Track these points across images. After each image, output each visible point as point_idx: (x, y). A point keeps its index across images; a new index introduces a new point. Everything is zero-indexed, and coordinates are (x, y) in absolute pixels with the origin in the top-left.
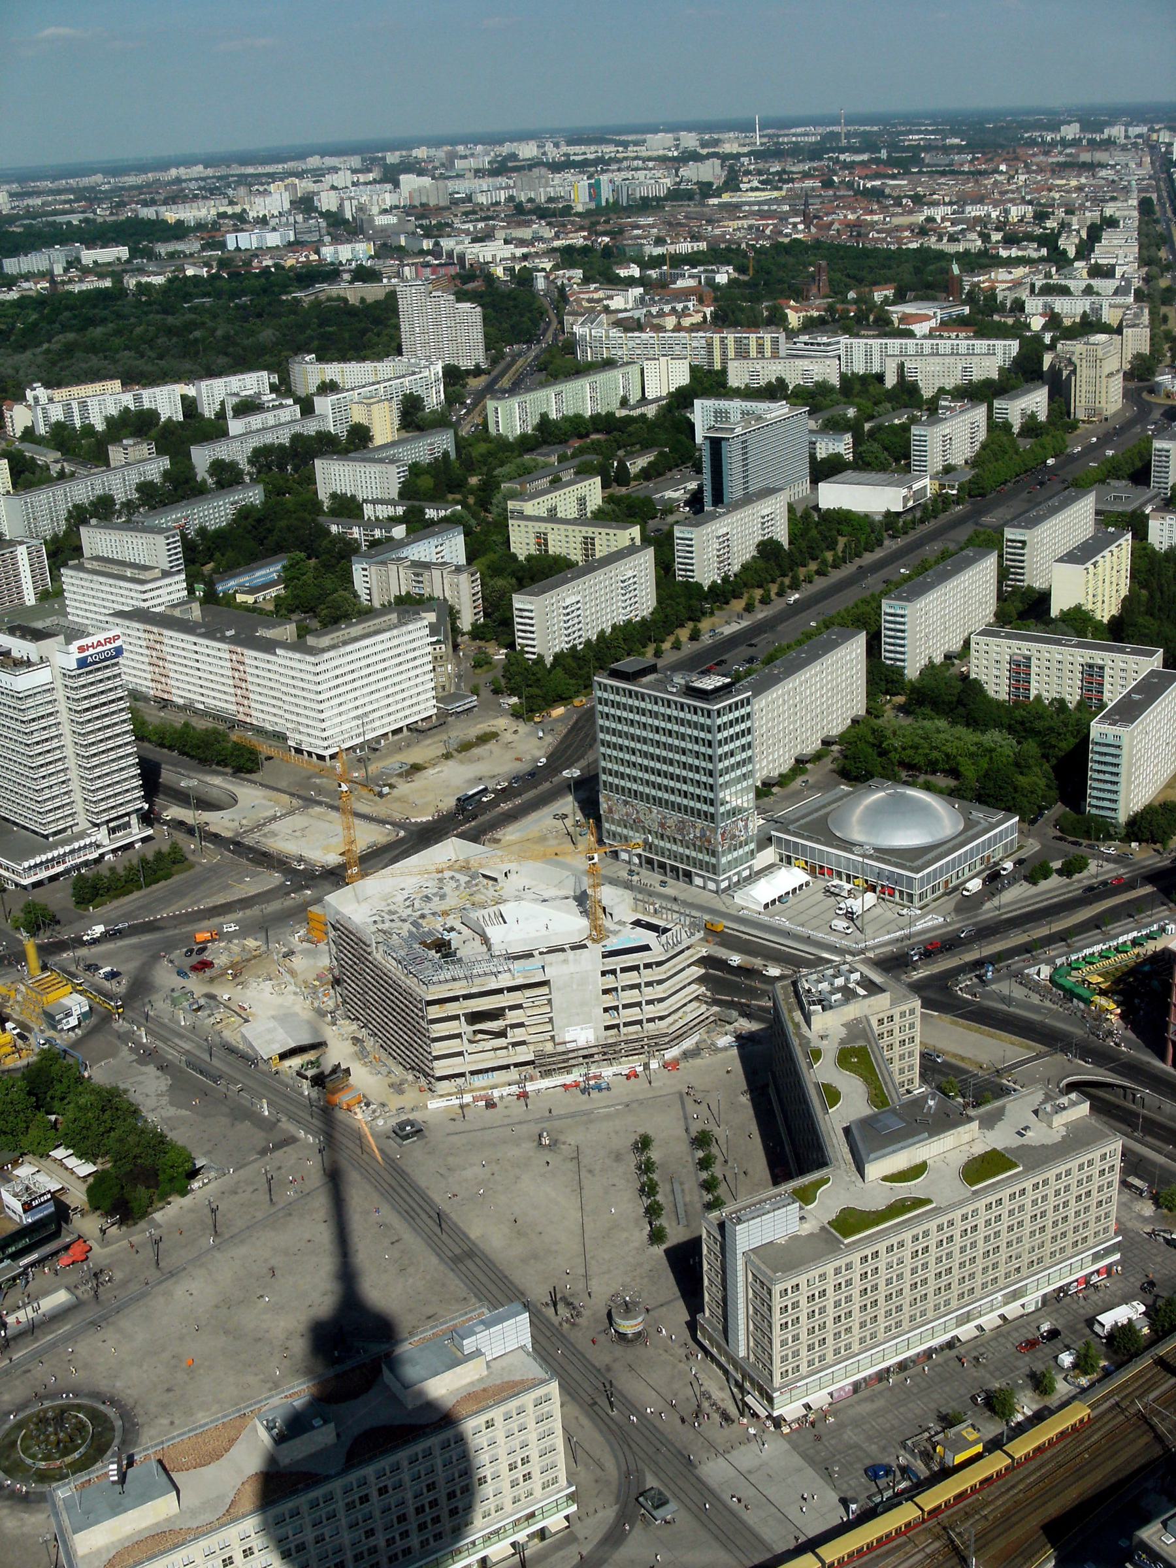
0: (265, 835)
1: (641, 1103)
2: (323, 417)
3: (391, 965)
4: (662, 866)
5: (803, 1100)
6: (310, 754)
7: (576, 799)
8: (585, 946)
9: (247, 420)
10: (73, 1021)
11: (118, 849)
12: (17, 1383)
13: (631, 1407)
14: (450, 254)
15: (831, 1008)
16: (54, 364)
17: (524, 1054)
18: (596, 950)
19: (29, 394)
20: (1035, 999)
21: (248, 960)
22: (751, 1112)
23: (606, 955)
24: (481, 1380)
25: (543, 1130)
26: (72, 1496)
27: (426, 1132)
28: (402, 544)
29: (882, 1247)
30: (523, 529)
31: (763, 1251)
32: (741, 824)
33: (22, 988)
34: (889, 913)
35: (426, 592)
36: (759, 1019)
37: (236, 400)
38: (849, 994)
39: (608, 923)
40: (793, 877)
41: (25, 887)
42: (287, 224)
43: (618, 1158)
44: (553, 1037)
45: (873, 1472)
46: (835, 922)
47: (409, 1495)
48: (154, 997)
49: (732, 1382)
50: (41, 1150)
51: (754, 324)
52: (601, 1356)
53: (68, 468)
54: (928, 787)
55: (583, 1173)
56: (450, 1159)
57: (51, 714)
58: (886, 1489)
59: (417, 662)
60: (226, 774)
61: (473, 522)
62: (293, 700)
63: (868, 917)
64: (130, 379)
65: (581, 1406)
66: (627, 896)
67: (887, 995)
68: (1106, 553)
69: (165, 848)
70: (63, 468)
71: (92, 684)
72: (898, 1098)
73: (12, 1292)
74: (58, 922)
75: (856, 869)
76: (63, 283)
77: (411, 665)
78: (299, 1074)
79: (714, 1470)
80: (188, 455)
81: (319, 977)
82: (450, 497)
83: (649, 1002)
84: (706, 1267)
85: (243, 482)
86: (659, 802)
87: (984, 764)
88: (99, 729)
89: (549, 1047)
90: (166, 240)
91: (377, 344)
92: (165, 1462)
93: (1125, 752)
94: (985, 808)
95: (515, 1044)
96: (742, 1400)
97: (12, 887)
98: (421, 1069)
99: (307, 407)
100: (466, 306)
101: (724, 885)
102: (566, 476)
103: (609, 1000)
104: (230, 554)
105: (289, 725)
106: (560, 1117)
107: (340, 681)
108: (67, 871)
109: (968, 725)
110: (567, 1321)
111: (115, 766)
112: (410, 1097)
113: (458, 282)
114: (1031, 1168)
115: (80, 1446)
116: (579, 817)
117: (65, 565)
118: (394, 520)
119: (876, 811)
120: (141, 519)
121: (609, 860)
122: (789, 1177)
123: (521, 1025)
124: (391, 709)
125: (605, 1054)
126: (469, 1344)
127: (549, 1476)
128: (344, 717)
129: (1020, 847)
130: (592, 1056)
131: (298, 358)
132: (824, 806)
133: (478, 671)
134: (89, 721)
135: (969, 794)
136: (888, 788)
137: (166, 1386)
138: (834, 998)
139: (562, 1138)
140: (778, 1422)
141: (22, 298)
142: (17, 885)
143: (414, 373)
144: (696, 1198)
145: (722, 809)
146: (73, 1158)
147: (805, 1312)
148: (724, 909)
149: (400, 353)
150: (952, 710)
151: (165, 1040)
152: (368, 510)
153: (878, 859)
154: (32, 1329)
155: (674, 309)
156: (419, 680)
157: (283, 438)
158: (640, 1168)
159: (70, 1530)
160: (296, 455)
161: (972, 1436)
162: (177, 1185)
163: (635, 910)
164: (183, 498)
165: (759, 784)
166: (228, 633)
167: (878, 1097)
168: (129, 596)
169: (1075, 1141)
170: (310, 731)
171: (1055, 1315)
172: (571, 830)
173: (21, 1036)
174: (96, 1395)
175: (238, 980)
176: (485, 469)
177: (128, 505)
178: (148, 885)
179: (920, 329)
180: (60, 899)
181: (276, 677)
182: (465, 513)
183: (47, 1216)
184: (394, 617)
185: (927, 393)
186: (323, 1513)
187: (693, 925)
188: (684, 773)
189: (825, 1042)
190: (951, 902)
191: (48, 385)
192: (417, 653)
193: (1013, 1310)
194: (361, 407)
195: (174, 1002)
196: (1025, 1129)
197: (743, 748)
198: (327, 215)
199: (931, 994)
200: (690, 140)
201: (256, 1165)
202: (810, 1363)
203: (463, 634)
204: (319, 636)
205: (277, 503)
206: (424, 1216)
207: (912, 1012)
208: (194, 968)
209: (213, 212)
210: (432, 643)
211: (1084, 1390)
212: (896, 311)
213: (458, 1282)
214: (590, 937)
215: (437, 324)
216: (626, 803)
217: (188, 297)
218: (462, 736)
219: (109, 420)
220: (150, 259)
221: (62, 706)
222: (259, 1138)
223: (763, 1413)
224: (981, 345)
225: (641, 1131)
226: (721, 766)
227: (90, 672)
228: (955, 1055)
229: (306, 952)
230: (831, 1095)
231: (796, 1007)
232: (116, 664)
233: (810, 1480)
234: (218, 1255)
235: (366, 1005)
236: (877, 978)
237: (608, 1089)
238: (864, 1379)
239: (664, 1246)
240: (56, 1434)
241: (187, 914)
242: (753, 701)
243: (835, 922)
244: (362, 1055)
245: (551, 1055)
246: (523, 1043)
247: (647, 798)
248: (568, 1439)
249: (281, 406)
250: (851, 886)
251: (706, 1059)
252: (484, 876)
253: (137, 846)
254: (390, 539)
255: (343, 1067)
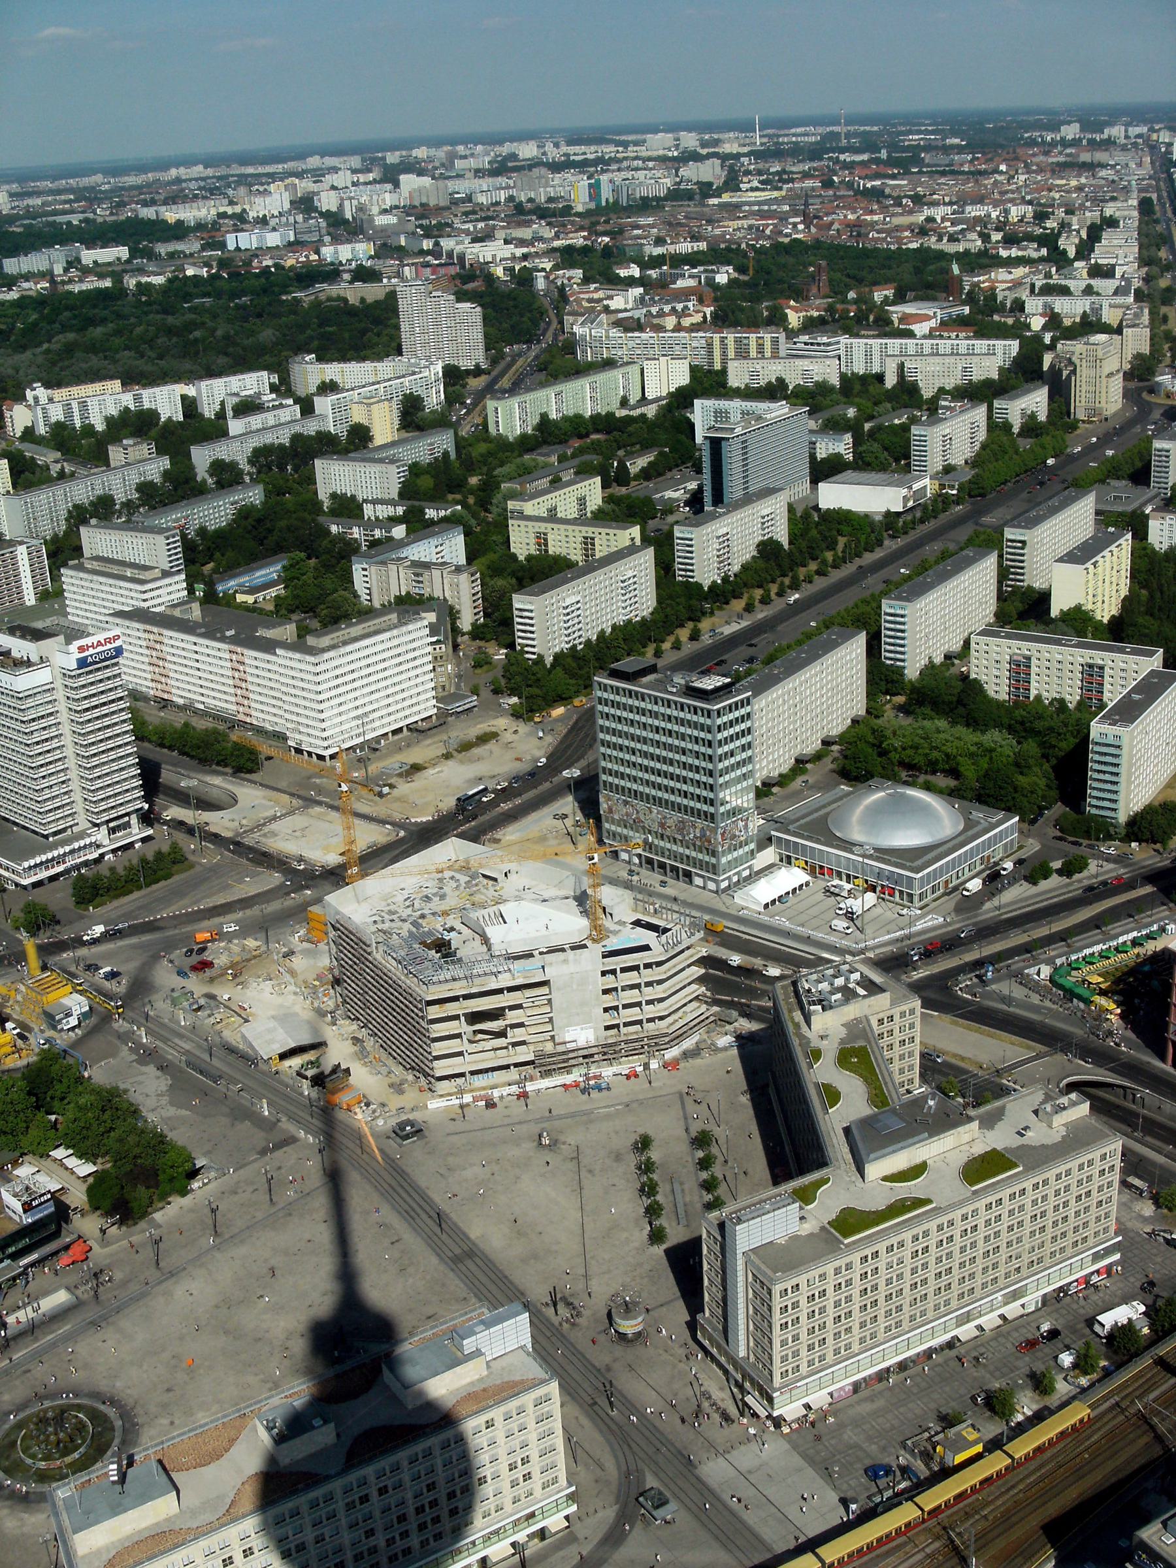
0: (265, 835)
1: (641, 1103)
2: (323, 417)
3: (391, 965)
4: (662, 866)
5: (803, 1100)
6: (310, 754)
7: (576, 799)
8: (585, 946)
9: (247, 420)
10: (73, 1021)
11: (118, 849)
12: (17, 1383)
13: (631, 1407)
14: (450, 254)
15: (831, 1008)
16: (54, 364)
17: (524, 1054)
18: (596, 950)
19: (29, 394)
20: (1035, 999)
21: (248, 960)
22: (751, 1112)
23: (606, 955)
24: (481, 1380)
25: (543, 1130)
26: (72, 1496)
27: (426, 1132)
28: (402, 544)
29: (882, 1247)
30: (523, 529)
31: (763, 1251)
32: (741, 824)
33: (22, 988)
34: (889, 913)
35: (426, 592)
36: (759, 1019)
37: (236, 400)
38: (849, 994)
39: (608, 923)
40: (793, 877)
41: (25, 887)
42: (287, 224)
43: (618, 1158)
44: (553, 1037)
45: (873, 1472)
46: (835, 922)
47: (409, 1495)
48: (154, 997)
49: (732, 1382)
50: (41, 1150)
51: (754, 324)
52: (601, 1356)
53: (68, 468)
54: (928, 787)
55: (583, 1173)
56: (450, 1159)
57: (51, 714)
58: (886, 1489)
59: (417, 662)
60: (226, 774)
61: (473, 522)
62: (293, 700)
63: (868, 917)
64: (130, 379)
65: (581, 1406)
66: (627, 896)
67: (887, 995)
68: (1106, 553)
69: (165, 848)
70: (63, 468)
71: (92, 684)
72: (898, 1098)
73: (12, 1292)
74: (58, 922)
75: (856, 869)
76: (63, 283)
77: (411, 665)
78: (299, 1074)
79: (714, 1470)
80: (188, 455)
81: (319, 977)
82: (450, 497)
83: (649, 1002)
84: (706, 1267)
85: (243, 482)
86: (659, 802)
87: (984, 764)
88: (99, 729)
89: (549, 1047)
90: (166, 240)
91: (377, 344)
92: (165, 1462)
93: (1125, 752)
94: (985, 808)
95: (515, 1044)
96: (742, 1400)
97: (12, 887)
98: (421, 1069)
99: (307, 407)
100: (466, 306)
101: (724, 885)
102: (566, 476)
103: (609, 1000)
104: (230, 554)
105: (289, 725)
106: (560, 1117)
107: (340, 681)
108: (67, 871)
109: (968, 725)
110: (567, 1321)
111: (115, 766)
112: (410, 1097)
113: (458, 282)
114: (1031, 1168)
115: (80, 1446)
116: (579, 817)
117: (65, 565)
118: (394, 520)
119: (876, 811)
120: (141, 519)
121: (609, 860)
122: (789, 1177)
123: (521, 1025)
124: (391, 709)
125: (605, 1054)
126: (469, 1344)
127: (549, 1476)
128: (344, 717)
129: (1020, 847)
130: (592, 1056)
131: (298, 358)
132: (824, 806)
133: (478, 671)
134: (89, 721)
135: (969, 794)
136: (888, 788)
137: (166, 1386)
138: (834, 998)
139: (562, 1138)
140: (778, 1422)
141: (22, 298)
142: (17, 885)
143: (414, 373)
144: (696, 1198)
145: (722, 809)
146: (73, 1158)
147: (805, 1312)
148: (724, 909)
149: (400, 353)
150: (952, 710)
151: (165, 1040)
152: (368, 510)
153: (878, 859)
154: (32, 1329)
155: (674, 309)
156: (419, 680)
157: (283, 438)
158: (640, 1168)
159: (70, 1530)
160: (296, 455)
161: (972, 1436)
162: (177, 1185)
163: (635, 910)
164: (183, 498)
165: (759, 784)
166: (228, 633)
167: (878, 1097)
168: (129, 596)
169: (1075, 1141)
170: (310, 731)
171: (1055, 1315)
172: (571, 830)
173: (21, 1036)
174: (96, 1395)
175: (238, 980)
176: (485, 469)
177: (128, 505)
178: (148, 885)
179: (920, 329)
180: (60, 899)
181: (276, 677)
182: (465, 513)
183: (47, 1216)
184: (394, 617)
185: (927, 393)
186: (323, 1513)
187: (693, 925)
188: (684, 773)
189: (825, 1042)
190: (951, 902)
191: (48, 385)
192: (417, 653)
193: (1013, 1310)
194: (361, 407)
195: (174, 1002)
196: (1025, 1129)
197: (743, 748)
198: (327, 215)
199: (931, 994)
200: (690, 140)
201: (256, 1165)
202: (810, 1363)
203: (463, 634)
204: (319, 636)
205: (277, 503)
206: (424, 1216)
207: (912, 1012)
208: (194, 968)
209: (213, 212)
210: (432, 643)
211: (1084, 1390)
212: (896, 311)
213: (458, 1282)
214: (590, 937)
215: (437, 324)
216: (626, 803)
217: (188, 297)
218: (462, 736)
219: (109, 420)
220: (150, 259)
221: (62, 706)
222: (259, 1138)
223: (763, 1413)
224: (981, 345)
225: (641, 1131)
226: (721, 766)
227: (90, 672)
228: (955, 1055)
229: (306, 952)
230: (831, 1095)
231: (796, 1007)
232: (116, 664)
233: (810, 1480)
234: (218, 1255)
235: (366, 1005)
236: (877, 978)
237: (608, 1089)
238: (864, 1379)
239: (664, 1246)
240: (56, 1434)
241: (187, 914)
242: (753, 701)
243: (835, 922)
244: (362, 1055)
245: (551, 1055)
246: (523, 1043)
247: (647, 798)
248: (568, 1439)
249: (281, 406)
250: (851, 886)
251: (706, 1059)
252: (484, 876)
253: (137, 846)
254: (390, 539)
255: (343, 1067)
